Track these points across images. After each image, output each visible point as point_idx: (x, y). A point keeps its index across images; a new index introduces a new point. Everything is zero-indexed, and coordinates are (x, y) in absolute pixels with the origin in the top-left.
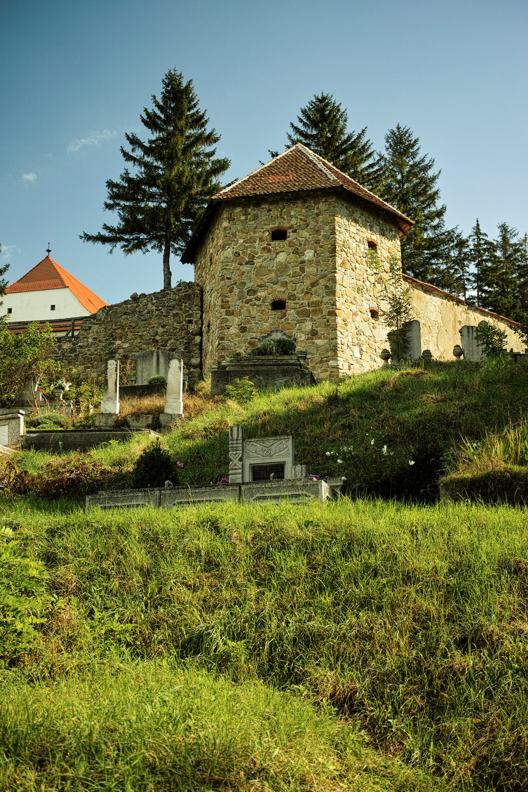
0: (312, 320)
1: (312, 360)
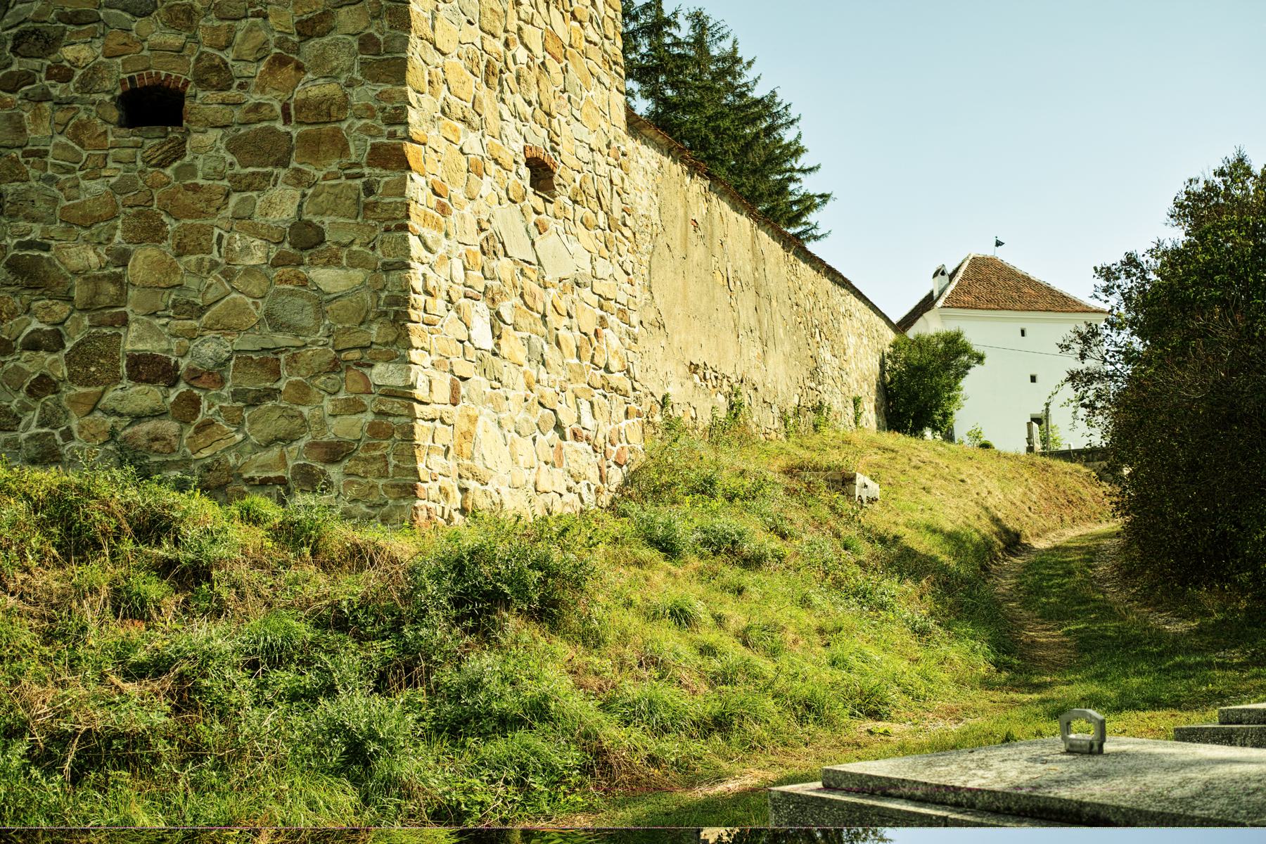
0: (299, 179)
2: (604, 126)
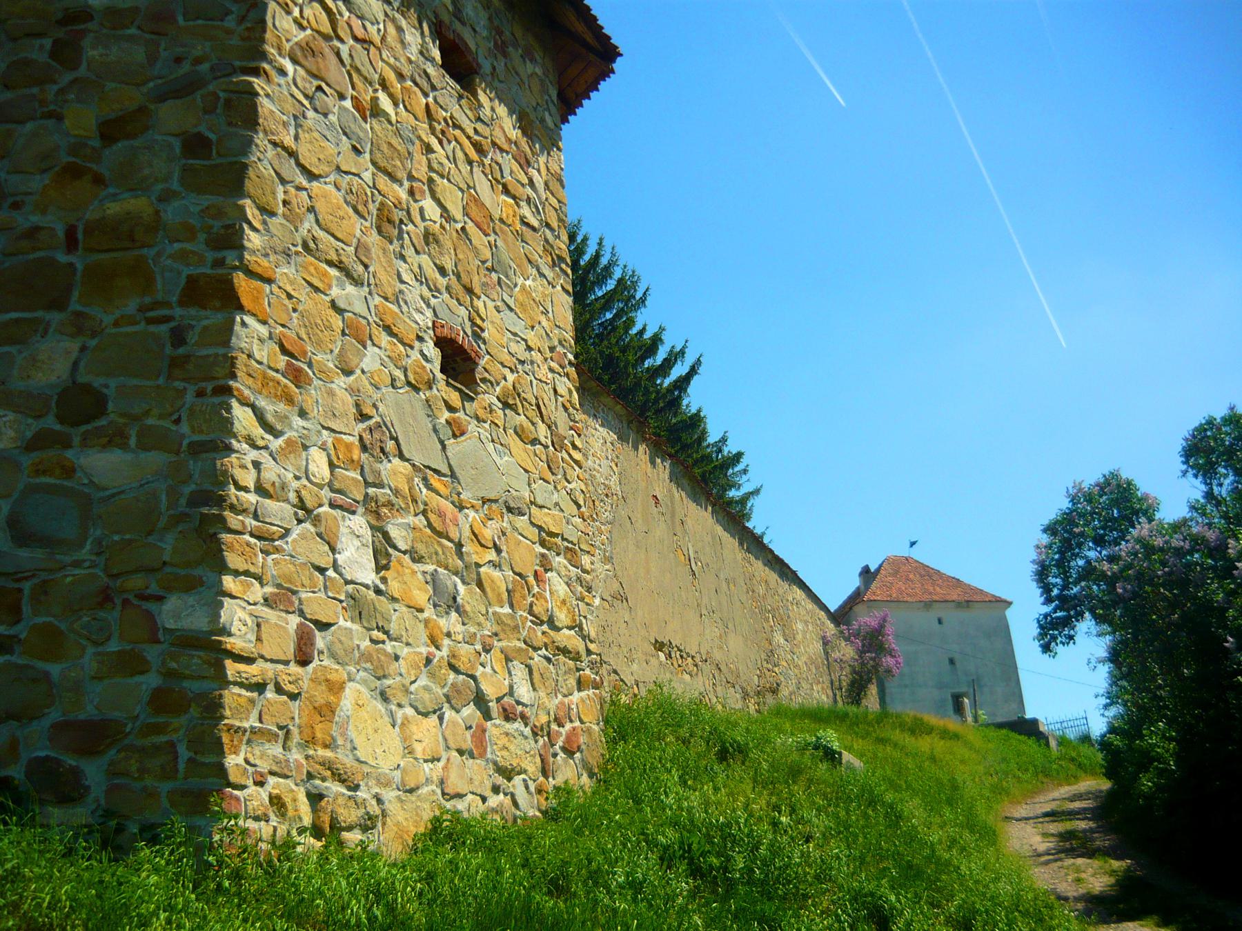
0: (80, 325)
1: (43, 589)
2: (545, 323)
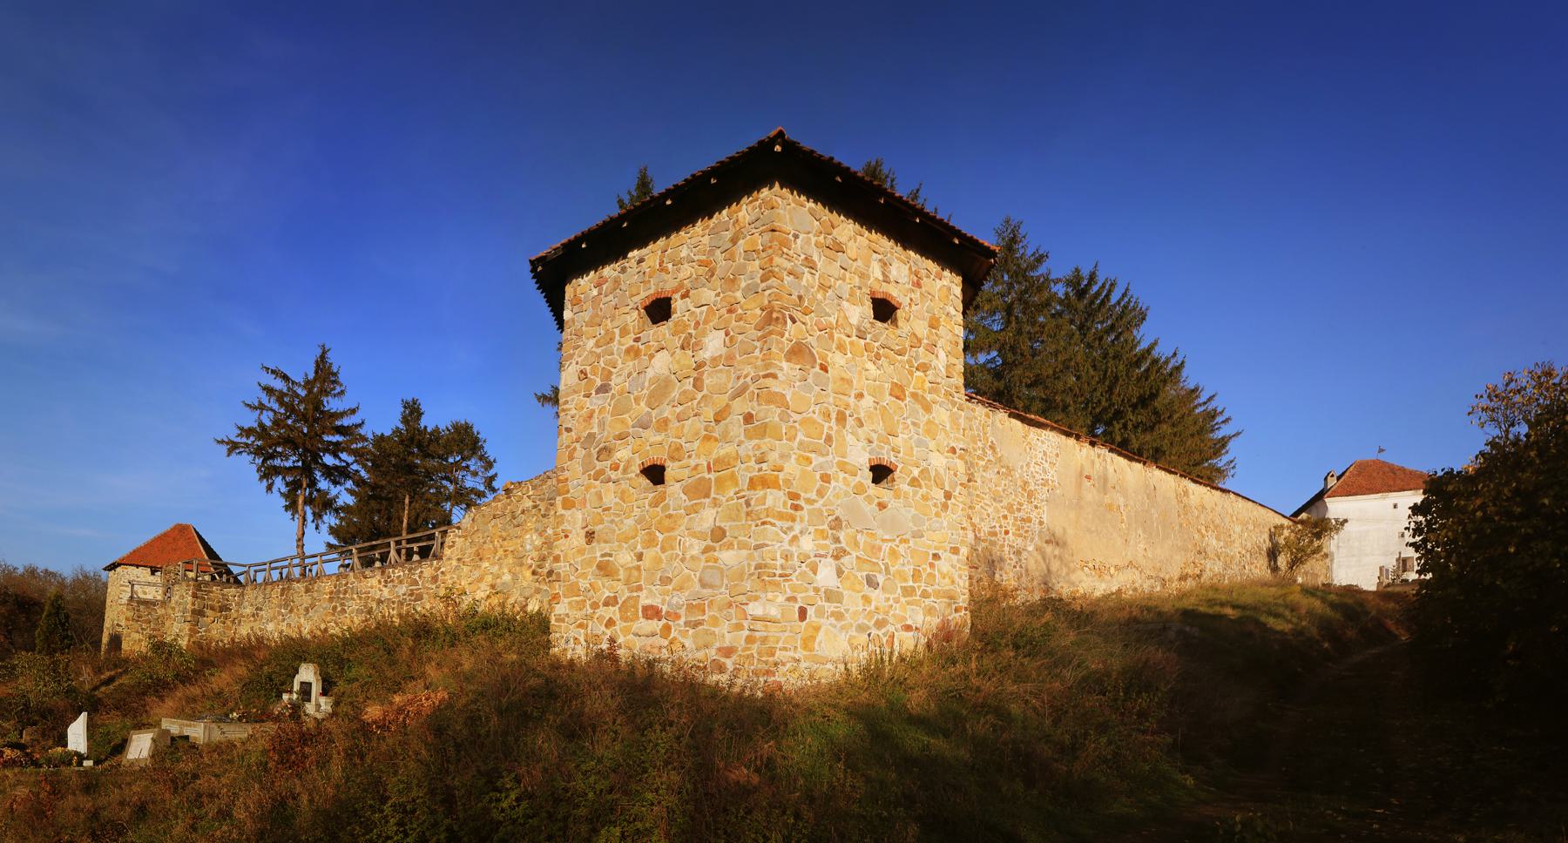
0: (716, 503)
